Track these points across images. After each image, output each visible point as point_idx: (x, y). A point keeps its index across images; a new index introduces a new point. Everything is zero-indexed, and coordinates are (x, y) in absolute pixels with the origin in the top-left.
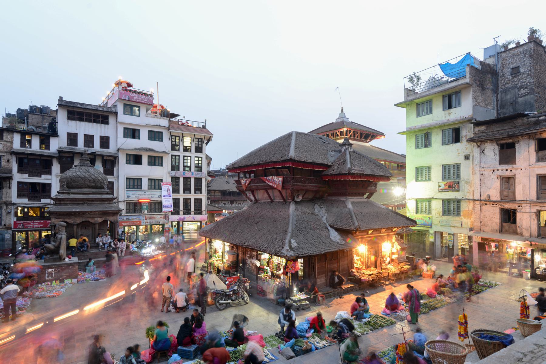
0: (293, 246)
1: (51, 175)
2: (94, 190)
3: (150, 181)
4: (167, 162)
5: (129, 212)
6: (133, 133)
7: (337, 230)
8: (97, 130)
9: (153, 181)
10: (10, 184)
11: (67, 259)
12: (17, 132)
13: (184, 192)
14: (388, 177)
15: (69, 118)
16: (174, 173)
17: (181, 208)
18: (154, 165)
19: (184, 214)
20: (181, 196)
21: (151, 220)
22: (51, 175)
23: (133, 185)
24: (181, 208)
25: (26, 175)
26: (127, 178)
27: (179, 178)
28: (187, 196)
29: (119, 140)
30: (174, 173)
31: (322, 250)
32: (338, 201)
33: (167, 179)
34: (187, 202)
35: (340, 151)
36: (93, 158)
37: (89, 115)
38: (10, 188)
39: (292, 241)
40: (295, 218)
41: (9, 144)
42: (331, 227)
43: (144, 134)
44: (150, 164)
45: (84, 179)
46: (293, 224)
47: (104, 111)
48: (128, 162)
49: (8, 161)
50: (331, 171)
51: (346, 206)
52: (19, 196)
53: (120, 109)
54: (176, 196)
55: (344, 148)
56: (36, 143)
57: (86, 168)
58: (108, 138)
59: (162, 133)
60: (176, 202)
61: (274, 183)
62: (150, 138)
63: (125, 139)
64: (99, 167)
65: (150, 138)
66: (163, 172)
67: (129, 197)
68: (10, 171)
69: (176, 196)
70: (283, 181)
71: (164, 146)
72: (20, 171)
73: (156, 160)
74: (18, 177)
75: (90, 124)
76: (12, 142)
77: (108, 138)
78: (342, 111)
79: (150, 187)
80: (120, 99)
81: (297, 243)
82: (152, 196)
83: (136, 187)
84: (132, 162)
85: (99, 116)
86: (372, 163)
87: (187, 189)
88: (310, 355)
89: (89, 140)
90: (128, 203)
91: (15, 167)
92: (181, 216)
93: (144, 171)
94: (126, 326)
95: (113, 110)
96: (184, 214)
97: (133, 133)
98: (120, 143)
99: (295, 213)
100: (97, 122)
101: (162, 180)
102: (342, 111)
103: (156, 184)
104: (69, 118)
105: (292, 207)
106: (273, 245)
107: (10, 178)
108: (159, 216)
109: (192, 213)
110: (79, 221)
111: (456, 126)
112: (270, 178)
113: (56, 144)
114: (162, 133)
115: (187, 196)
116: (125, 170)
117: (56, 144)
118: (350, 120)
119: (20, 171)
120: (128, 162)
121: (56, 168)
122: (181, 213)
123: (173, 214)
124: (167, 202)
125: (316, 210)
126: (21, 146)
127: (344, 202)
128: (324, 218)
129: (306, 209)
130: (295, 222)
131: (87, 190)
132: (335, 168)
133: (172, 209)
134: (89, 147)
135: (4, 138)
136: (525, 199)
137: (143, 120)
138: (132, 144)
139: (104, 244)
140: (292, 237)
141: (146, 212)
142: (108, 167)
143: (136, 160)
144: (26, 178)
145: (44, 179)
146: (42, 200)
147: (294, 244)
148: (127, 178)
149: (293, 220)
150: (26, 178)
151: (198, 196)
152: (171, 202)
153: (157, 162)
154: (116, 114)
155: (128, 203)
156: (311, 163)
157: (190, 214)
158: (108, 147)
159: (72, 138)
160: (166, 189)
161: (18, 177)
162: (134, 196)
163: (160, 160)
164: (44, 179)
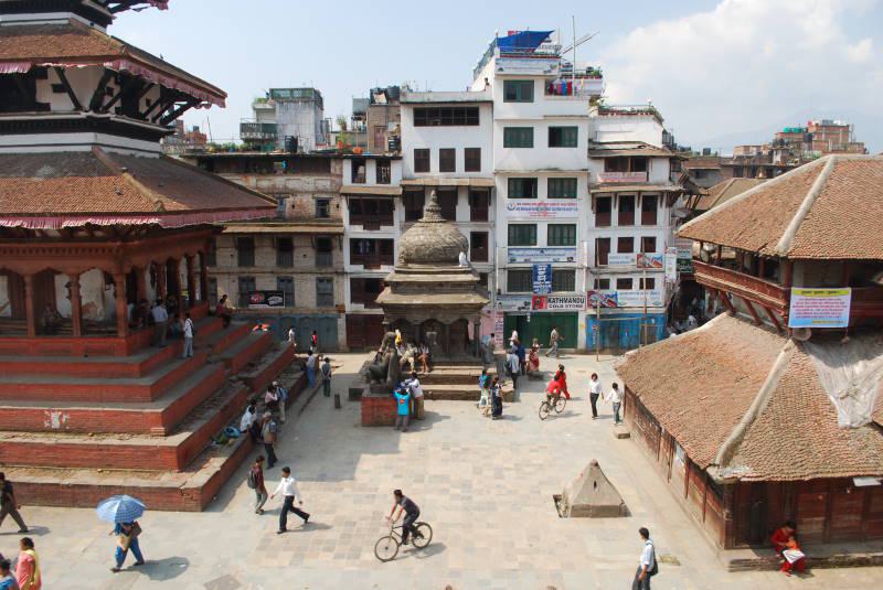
3: (512, 228)
9: (558, 229)
15: (418, 123)
26: (509, 225)
36: (447, 200)
38: (341, 248)
41: (337, 180)
52: (353, 261)
56: (370, 171)
59: (576, 128)
72: (353, 221)
75: (462, 128)
76: (341, 176)
79: (552, 241)
82: (556, 257)
83: (565, 241)
84: (519, 194)
93: (542, 212)
94: (424, 449)
97: (518, 137)
98: (500, 161)
104: (418, 123)
111: (324, 196)
113: (402, 173)
116: (506, 212)
119: (353, 221)
121: (399, 213)
135: (332, 170)
144: (358, 232)
145: (383, 233)
148: (509, 225)
150: (358, 232)
159: (422, 160)
163: (572, 184)
164: (383, 233)
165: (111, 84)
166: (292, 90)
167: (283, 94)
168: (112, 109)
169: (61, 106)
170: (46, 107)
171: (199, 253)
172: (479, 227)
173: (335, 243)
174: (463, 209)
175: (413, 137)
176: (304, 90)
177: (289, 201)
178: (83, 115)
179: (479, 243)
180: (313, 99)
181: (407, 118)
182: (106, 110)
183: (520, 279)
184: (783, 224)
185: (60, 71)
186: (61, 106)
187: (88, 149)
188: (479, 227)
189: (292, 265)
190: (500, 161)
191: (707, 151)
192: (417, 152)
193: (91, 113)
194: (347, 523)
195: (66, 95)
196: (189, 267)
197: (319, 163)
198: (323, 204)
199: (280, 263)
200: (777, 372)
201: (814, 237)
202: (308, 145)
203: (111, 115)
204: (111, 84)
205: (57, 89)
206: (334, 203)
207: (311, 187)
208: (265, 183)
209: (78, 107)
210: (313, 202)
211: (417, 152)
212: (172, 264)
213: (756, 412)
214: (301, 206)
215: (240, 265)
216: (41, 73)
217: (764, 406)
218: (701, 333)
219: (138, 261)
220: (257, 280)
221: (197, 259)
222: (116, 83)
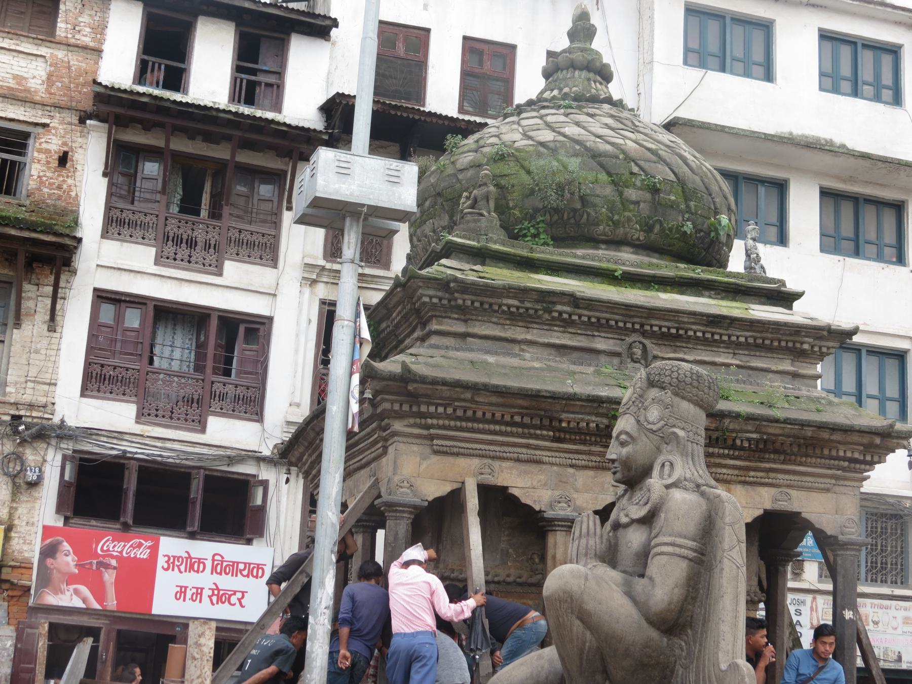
1: (274, 262)
10: (54, 298)
22: (274, 262)
41: (76, 60)
49: (63, 159)
62: (831, 81)
63: (696, 73)
65: (831, 81)
74: (112, 262)
91: (90, 192)
119: (116, 224)
126: (234, 97)
136: (12, 354)
145: (232, 288)
146: (214, 423)
153: (869, 231)
161: (112, 262)
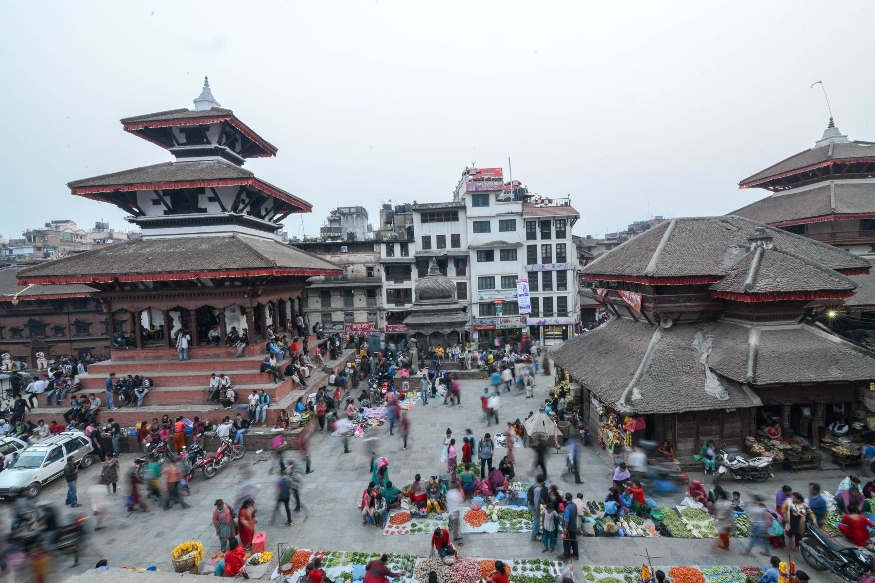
0: (633, 398)
2: (443, 300)
4: (522, 254)
5: (483, 315)
6: (482, 226)
7: (722, 378)
8: (445, 229)
11: (419, 373)
12: (383, 242)
13: (544, 290)
14: (851, 290)
15: (424, 221)
16: (530, 268)
17: (541, 309)
18: (508, 260)
19: (545, 316)
20: (541, 294)
21: (506, 324)
23: (486, 285)
24: (541, 309)
25: (392, 282)
27: (536, 273)
28: (548, 294)
29: (469, 236)
30: (530, 268)
31: (681, 407)
32: (737, 327)
33: (523, 276)
34: (548, 301)
35: (748, 249)
36: (442, 263)
37: (439, 214)
39: (636, 391)
40: (652, 356)
42: (712, 370)
43: (495, 225)
44: (502, 259)
45: (433, 289)
46: (645, 365)
47: (453, 208)
48: (479, 260)
50: (721, 286)
51: (747, 341)
52: (389, 302)
53: (469, 202)
54: (534, 294)
55: (754, 244)
56: (397, 248)
57: (435, 278)
58: (458, 236)
59: (515, 220)
60: (534, 302)
61: (632, 301)
64: (451, 270)
66: (519, 267)
67: (482, 298)
68: (380, 280)
69: (534, 294)
70: (643, 301)
71: (519, 235)
72: (388, 279)
73: (509, 253)
74: (388, 285)
75: (442, 223)
77: (458, 236)
78: (831, 125)
79: (504, 286)
80: (468, 192)
81: (642, 394)
85: (449, 213)
86: (809, 268)
87: (547, 286)
88: (613, 541)
89: (441, 240)
90: (482, 305)
92: (541, 319)
93: (498, 268)
95: (462, 204)
96: (545, 316)
97: (482, 226)
99: (657, 347)
100: (447, 220)
101: (516, 277)
102: (831, 125)
103: (510, 281)
104: (424, 221)
105: (657, 336)
106: (611, 392)
107: (380, 287)
108: (515, 319)
109: (555, 315)
110: (430, 332)
112: (627, 293)
113: (415, 249)
114: (515, 220)
115: (548, 294)
116: (477, 269)
117: (415, 249)
118: (851, 139)
119: (388, 279)
120: (479, 260)
121: (414, 273)
122: (541, 315)
123: (531, 315)
124: (524, 302)
125: (696, 342)
127: (747, 331)
128: (705, 356)
129: (675, 339)
130: (649, 362)
131: (436, 301)
132: (729, 281)
133: (530, 310)
134: (441, 247)
137: (494, 209)
138: (483, 239)
139: (453, 356)
140: (635, 385)
141: (501, 314)
142: (460, 266)
143: (486, 255)
145: (405, 285)
147: (636, 395)
149: (648, 357)
150: (392, 285)
151: (562, 294)
152: (529, 303)
154: (464, 208)
155: (482, 305)
156: (684, 277)
157: (552, 315)
158: (459, 246)
159: (426, 241)
160: (522, 286)
162: (486, 297)
164: (405, 285)
165: (243, 196)
166: (350, 208)
167: (345, 211)
168: (245, 211)
169: (214, 211)
170: (204, 210)
171: (298, 298)
172: (461, 280)
173: (378, 292)
174: (451, 270)
175: (421, 229)
176: (357, 208)
177: (350, 268)
178: (227, 214)
179: (462, 290)
180: (361, 213)
181: (417, 218)
182: (241, 211)
183: (488, 308)
184: (649, 258)
185: (213, 189)
186: (214, 211)
187: (231, 234)
188: (461, 280)
189: (353, 305)
190: (471, 239)
191: (589, 237)
192: (424, 238)
193: (232, 213)
194: (391, 453)
195: (217, 203)
196: (292, 307)
197: (367, 246)
198: (370, 269)
199: (345, 304)
200: (652, 348)
201: (669, 263)
202: (360, 238)
203: (244, 214)
204: (243, 196)
205: (211, 200)
206: (376, 269)
207: (363, 260)
208: (336, 258)
209: (224, 210)
210: (364, 268)
211: (424, 238)
212: (282, 303)
213: (643, 371)
214: (357, 271)
215: (322, 306)
216: (202, 191)
217: (647, 367)
218: (600, 330)
219: (263, 300)
220: (333, 315)
221: (297, 302)
222: (247, 197)
